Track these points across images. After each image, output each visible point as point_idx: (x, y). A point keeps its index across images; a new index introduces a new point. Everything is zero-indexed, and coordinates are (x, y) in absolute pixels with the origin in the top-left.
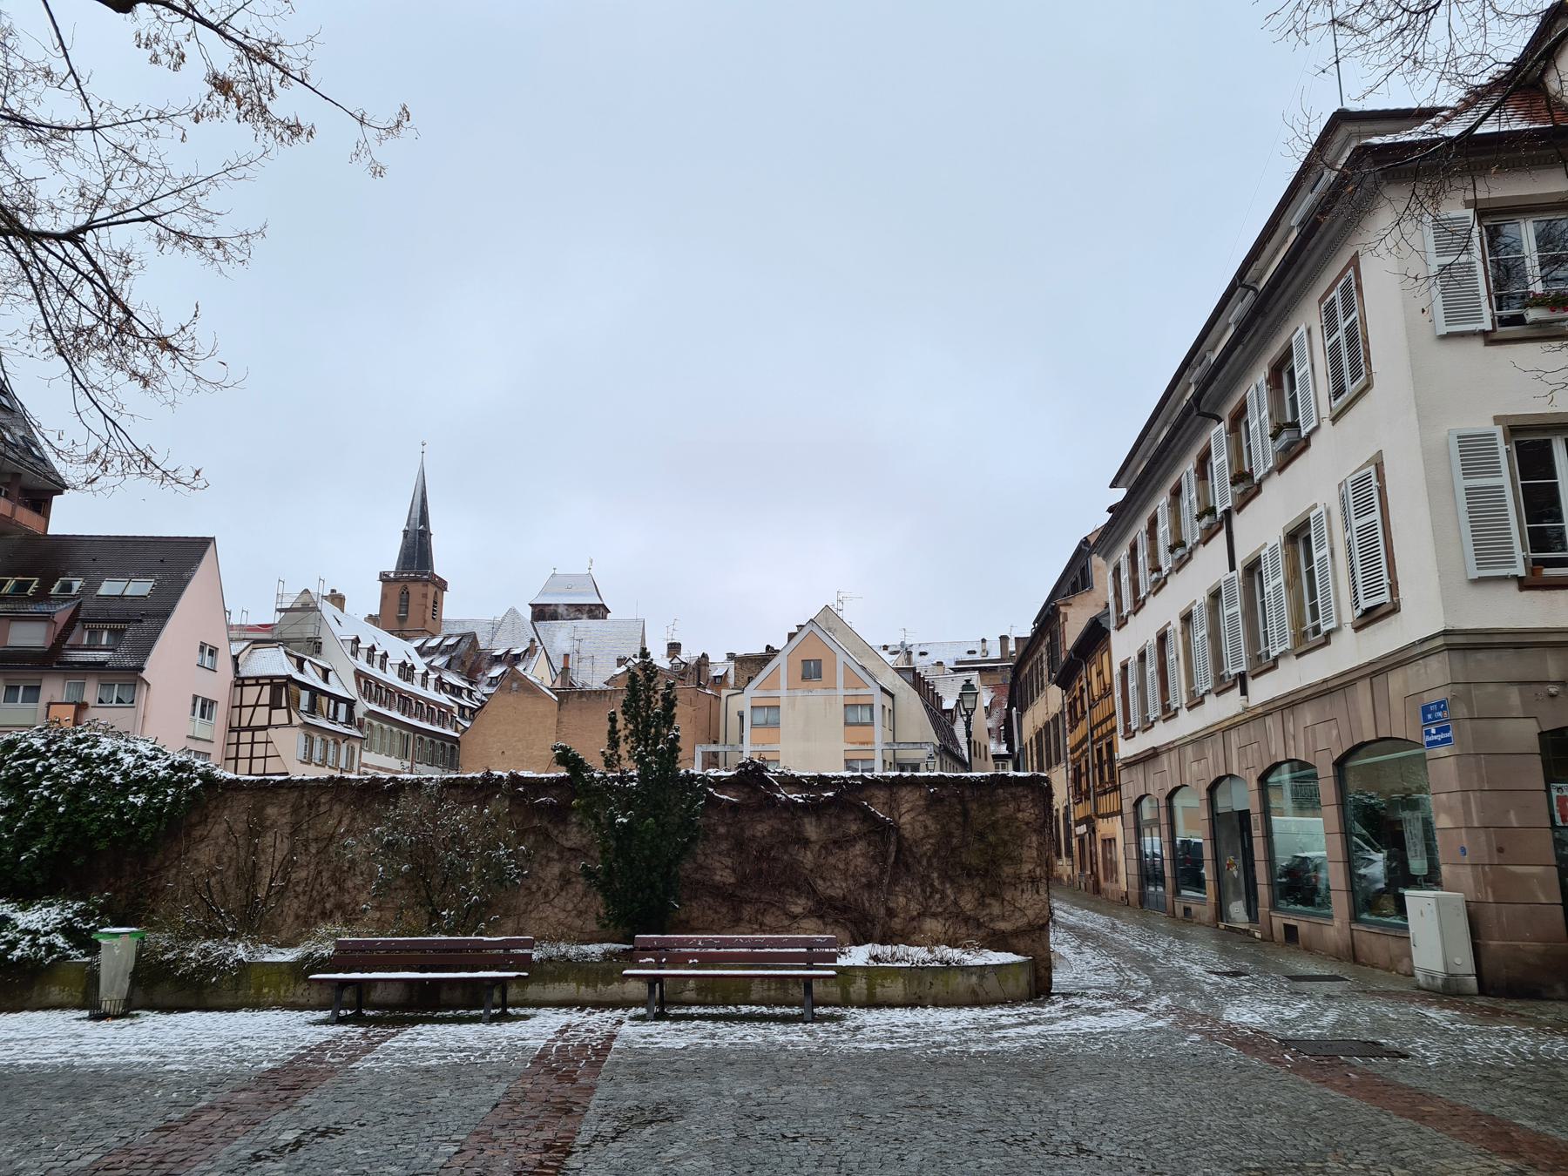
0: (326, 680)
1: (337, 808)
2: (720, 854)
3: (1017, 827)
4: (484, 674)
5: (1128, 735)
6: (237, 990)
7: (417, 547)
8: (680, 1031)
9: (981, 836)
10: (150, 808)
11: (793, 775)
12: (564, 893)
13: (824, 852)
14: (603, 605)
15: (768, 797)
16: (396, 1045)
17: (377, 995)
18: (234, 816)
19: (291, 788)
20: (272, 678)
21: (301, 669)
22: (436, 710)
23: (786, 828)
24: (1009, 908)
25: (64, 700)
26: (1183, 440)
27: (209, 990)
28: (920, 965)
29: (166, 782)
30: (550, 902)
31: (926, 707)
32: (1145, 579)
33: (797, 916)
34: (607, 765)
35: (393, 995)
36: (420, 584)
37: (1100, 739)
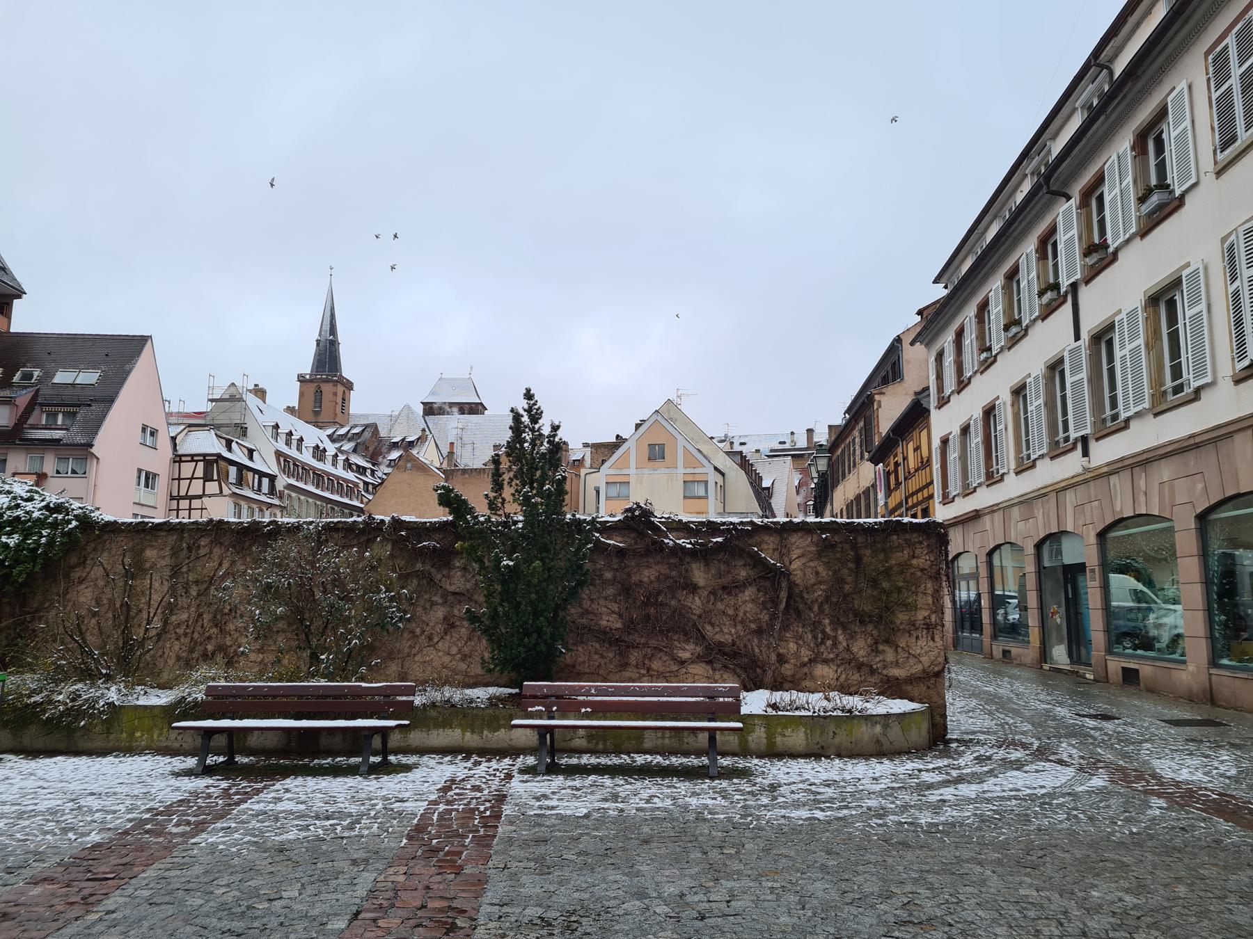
0: (251, 458)
1: (217, 551)
2: (606, 599)
3: (912, 574)
4: (384, 457)
5: (947, 501)
6: (109, 733)
7: (328, 355)
8: (578, 789)
9: (874, 583)
10: (24, 549)
11: (680, 521)
12: (448, 637)
13: (712, 598)
14: (481, 404)
15: (654, 542)
16: (256, 807)
17: (253, 741)
18: (110, 559)
19: (171, 530)
20: (204, 455)
21: (229, 449)
22: (345, 485)
23: (674, 573)
24: (903, 655)
25: (27, 471)
26: (1024, 223)
27: (79, 734)
28: (822, 714)
29: (40, 523)
30: (434, 646)
31: (751, 483)
32: (971, 357)
33: (686, 662)
34: (491, 508)
35: (271, 742)
36: (331, 384)
37: (914, 506)
